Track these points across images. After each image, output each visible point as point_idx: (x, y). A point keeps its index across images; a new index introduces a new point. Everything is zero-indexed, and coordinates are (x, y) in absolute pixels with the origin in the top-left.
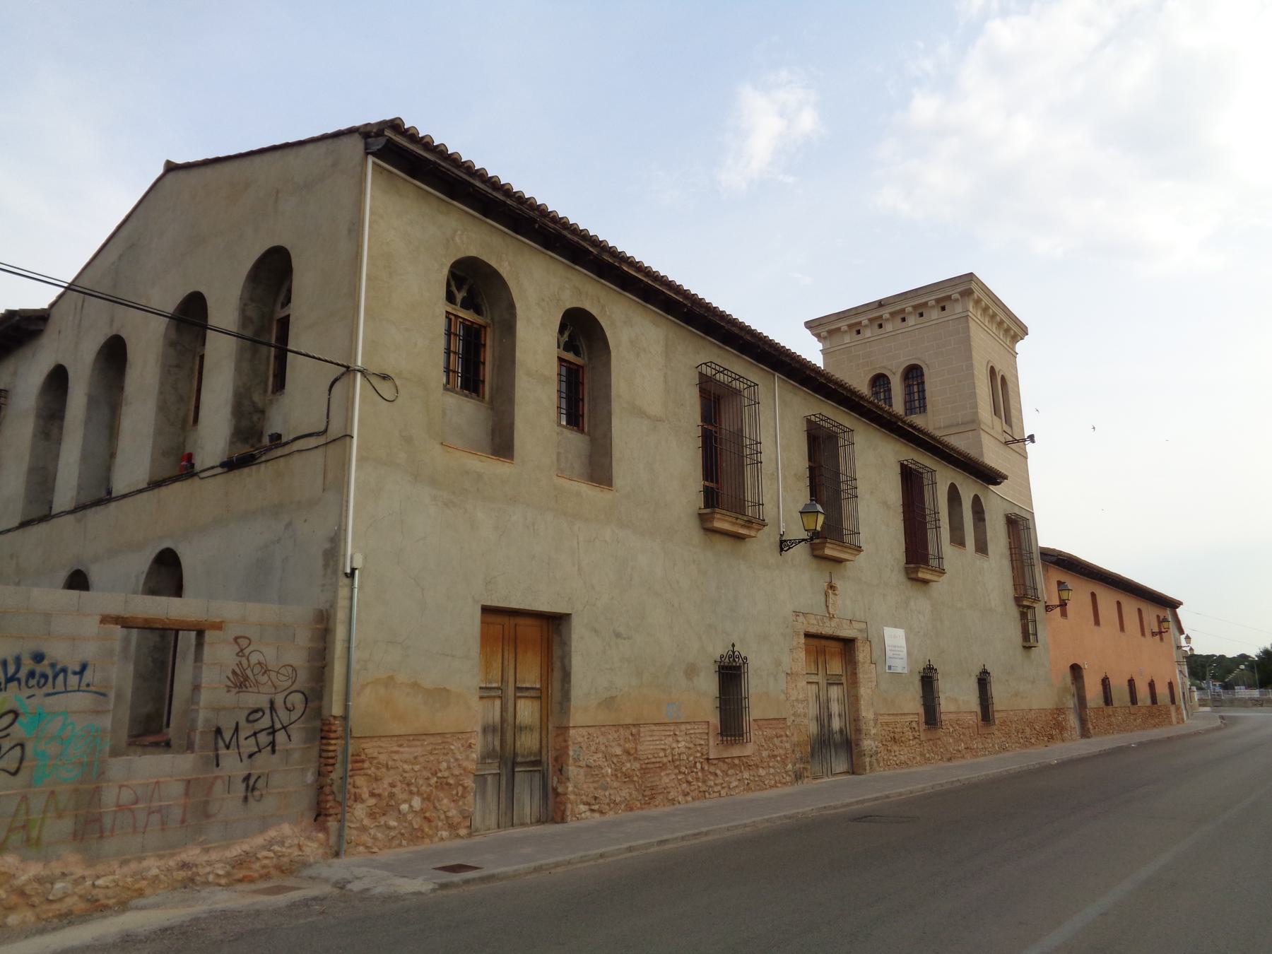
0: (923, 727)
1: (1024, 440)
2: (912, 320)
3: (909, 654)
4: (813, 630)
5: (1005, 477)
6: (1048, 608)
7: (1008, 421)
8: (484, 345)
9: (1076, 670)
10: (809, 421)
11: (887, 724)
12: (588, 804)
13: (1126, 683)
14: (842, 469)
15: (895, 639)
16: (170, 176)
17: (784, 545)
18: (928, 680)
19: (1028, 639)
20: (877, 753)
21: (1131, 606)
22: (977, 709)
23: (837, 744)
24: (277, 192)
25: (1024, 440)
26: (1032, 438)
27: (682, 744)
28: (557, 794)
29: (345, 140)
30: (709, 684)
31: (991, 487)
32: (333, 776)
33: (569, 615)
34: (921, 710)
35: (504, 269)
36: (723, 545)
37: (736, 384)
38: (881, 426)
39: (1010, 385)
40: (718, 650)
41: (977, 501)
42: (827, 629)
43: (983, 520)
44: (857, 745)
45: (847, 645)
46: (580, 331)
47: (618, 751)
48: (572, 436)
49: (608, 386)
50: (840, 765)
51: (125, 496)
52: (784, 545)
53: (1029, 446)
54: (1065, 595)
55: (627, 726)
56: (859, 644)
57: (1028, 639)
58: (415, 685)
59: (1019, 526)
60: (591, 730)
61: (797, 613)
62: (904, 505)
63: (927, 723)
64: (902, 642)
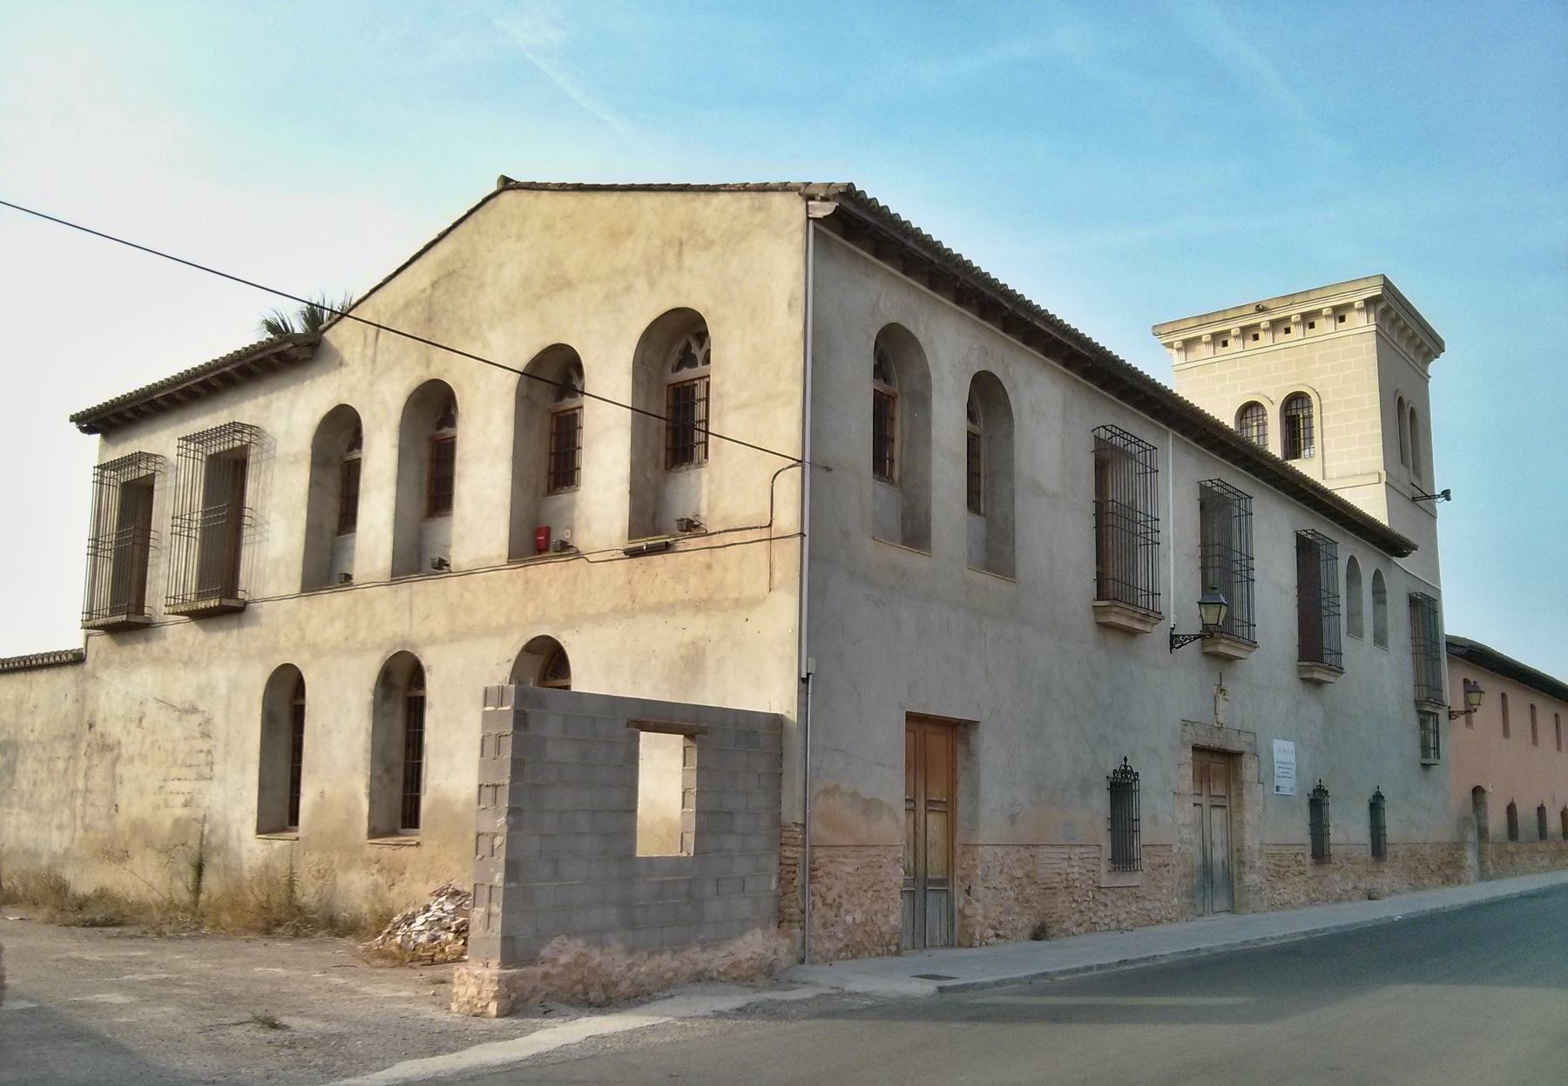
0: (1309, 860)
1: (1434, 497)
2: (1297, 332)
3: (1298, 772)
4: (1201, 743)
5: (1414, 548)
6: (1452, 715)
7: (1417, 472)
8: (893, 419)
9: (1478, 792)
10: (1203, 488)
11: (1273, 855)
12: (994, 928)
13: (1534, 813)
14: (1236, 545)
15: (1283, 751)
16: (508, 196)
17: (1175, 641)
18: (1318, 801)
19: (1429, 750)
20: (1261, 889)
21: (1520, 701)
22: (1367, 840)
23: (1216, 882)
24: (681, 244)
25: (1434, 497)
26: (1446, 494)
27: (1076, 869)
28: (964, 916)
29: (777, 199)
30: (1101, 802)
31: (1395, 559)
32: (796, 882)
33: (976, 723)
34: (1308, 840)
35: (921, 334)
36: (1115, 641)
37: (1132, 448)
38: (1247, 469)
39: (1420, 418)
40: (1112, 765)
41: (1377, 576)
42: (1215, 743)
43: (1383, 602)
44: (1240, 879)
45: (1230, 758)
46: (986, 395)
47: (1019, 873)
48: (883, 489)
49: (1010, 461)
50: (1221, 902)
51: (469, 573)
52: (1175, 641)
53: (1441, 506)
54: (1474, 698)
55: (1027, 846)
56: (1245, 759)
57: (1429, 750)
58: (855, 795)
59: (1424, 607)
60: (997, 849)
61: (1185, 722)
62: (1299, 587)
63: (1314, 855)
64: (1291, 758)
